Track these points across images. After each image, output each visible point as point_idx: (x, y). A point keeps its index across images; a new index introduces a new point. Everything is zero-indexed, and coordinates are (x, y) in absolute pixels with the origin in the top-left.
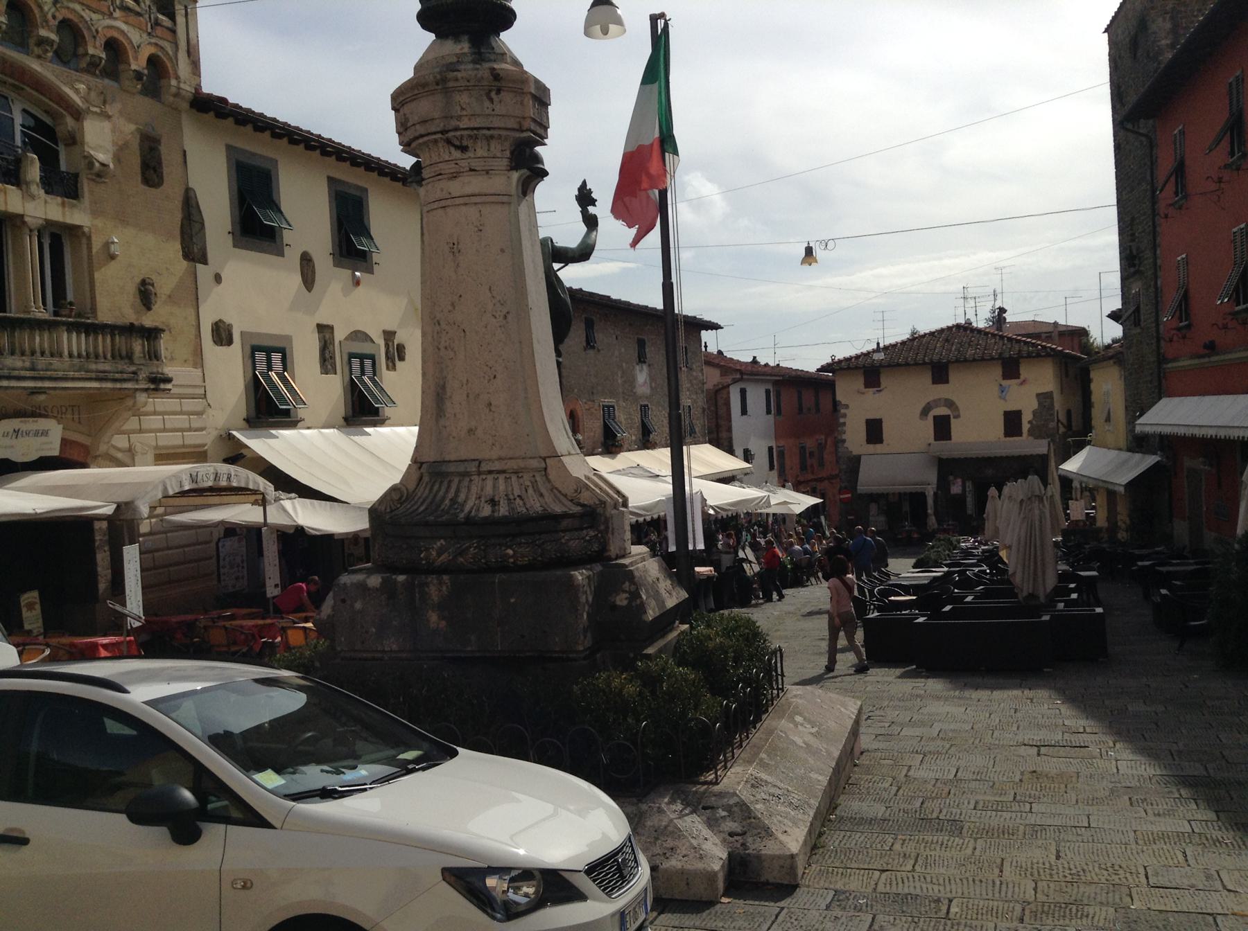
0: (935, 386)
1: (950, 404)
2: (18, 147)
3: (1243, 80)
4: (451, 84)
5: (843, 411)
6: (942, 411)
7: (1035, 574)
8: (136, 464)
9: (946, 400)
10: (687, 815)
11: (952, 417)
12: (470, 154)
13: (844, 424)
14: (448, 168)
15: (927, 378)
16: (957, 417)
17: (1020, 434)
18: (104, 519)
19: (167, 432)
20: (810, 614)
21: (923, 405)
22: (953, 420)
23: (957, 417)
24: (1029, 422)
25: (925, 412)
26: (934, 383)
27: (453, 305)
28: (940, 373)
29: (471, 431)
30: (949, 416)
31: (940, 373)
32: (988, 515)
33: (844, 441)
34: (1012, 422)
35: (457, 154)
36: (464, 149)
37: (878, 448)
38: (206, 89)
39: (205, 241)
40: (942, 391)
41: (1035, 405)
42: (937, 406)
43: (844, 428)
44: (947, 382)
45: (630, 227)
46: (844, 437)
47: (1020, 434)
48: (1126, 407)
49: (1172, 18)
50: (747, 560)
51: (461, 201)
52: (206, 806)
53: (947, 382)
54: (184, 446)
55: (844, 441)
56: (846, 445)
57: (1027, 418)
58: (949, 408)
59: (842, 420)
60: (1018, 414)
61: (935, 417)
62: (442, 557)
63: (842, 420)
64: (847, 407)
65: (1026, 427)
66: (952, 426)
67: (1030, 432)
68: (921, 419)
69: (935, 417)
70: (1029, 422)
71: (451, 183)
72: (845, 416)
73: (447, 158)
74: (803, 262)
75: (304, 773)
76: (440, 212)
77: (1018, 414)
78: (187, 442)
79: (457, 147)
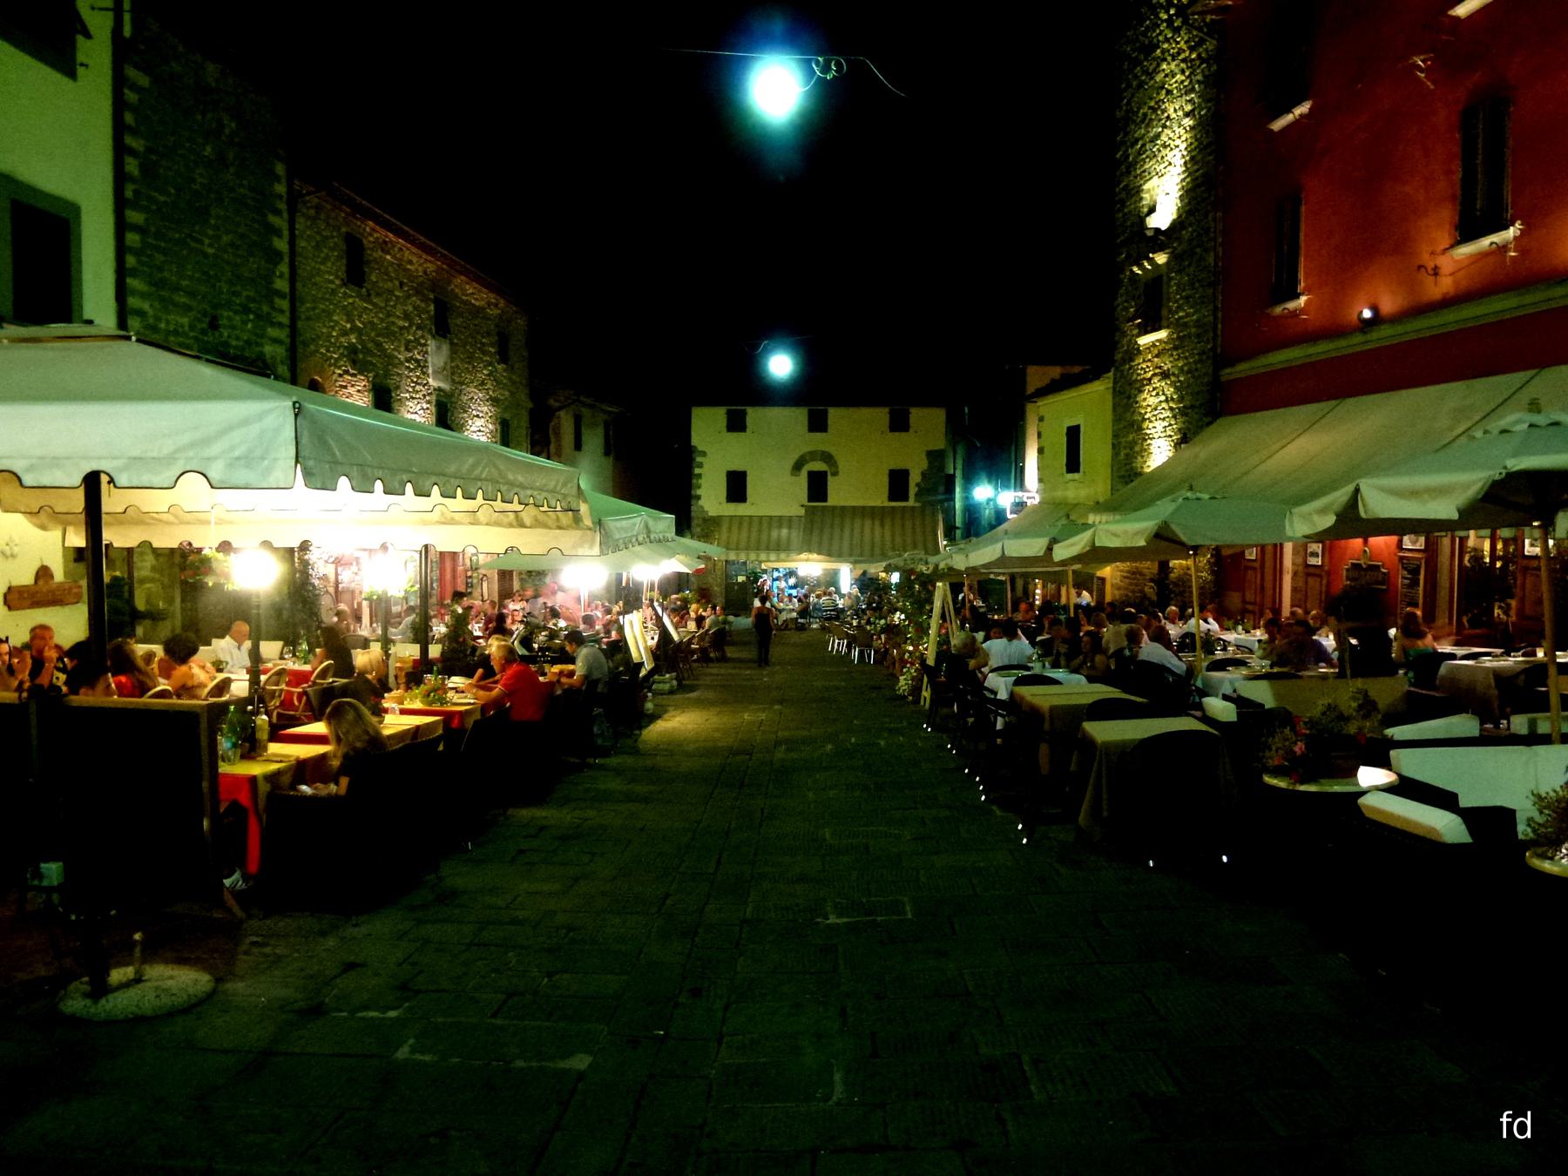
0: (729, 433)
1: (827, 458)
2: (479, 637)
5: (699, 459)
6: (818, 466)
7: (426, 558)
9: (823, 452)
10: (1020, 621)
11: (829, 474)
17: (906, 498)
18: (843, 511)
20: (406, 569)
22: (830, 478)
23: (835, 474)
25: (797, 467)
32: (1212, 539)
33: (699, 497)
39: (18, 609)
40: (818, 441)
41: (924, 464)
42: (812, 460)
43: (700, 481)
46: (699, 492)
47: (906, 498)
52: (1415, 674)
55: (699, 497)
57: (915, 478)
58: (825, 462)
59: (697, 471)
64: (704, 454)
65: (913, 490)
66: (829, 483)
68: (792, 475)
70: (917, 485)
75: (1108, 642)
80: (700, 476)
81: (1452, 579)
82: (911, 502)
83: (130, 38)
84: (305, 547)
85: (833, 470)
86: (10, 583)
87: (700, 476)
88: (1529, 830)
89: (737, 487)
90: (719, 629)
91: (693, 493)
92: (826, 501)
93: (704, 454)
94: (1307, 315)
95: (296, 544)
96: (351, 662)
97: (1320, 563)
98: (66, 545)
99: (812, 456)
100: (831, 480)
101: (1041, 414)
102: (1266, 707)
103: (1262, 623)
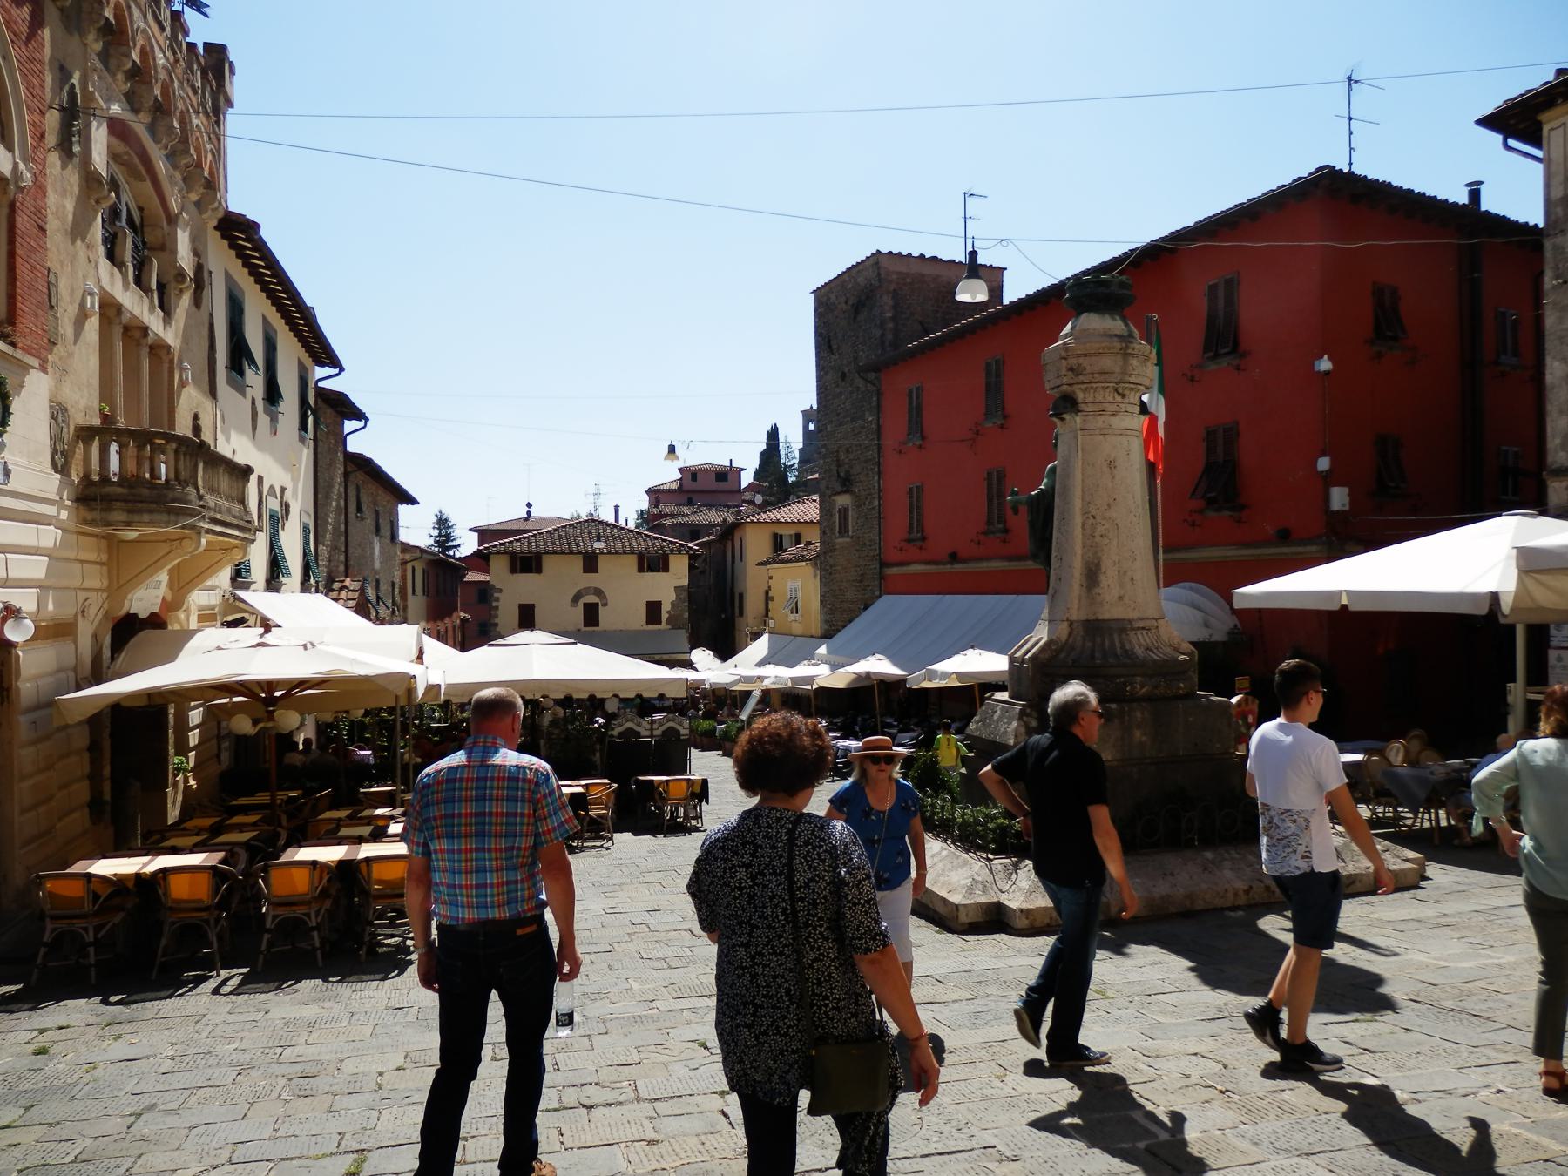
1: (599, 592)
3: (1004, 362)
4: (1130, 351)
8: (409, 621)
9: (595, 589)
12: (1126, 400)
13: (497, 608)
14: (1113, 408)
16: (605, 605)
17: (660, 623)
21: (574, 592)
23: (605, 605)
25: (576, 599)
27: (1109, 505)
29: (1121, 598)
30: (597, 604)
33: (497, 625)
34: (653, 609)
36: (1123, 396)
38: (231, 209)
40: (591, 580)
41: (673, 597)
46: (496, 621)
47: (660, 623)
49: (893, 298)
50: (815, 725)
51: (1119, 432)
55: (497, 625)
56: (498, 629)
57: (666, 608)
62: (1144, 690)
63: (494, 604)
64: (500, 591)
65: (665, 616)
67: (669, 621)
71: (1112, 418)
72: (497, 600)
73: (1111, 400)
74: (666, 458)
76: (1101, 437)
79: (1119, 394)
80: (497, 608)
82: (663, 626)
83: (1334, 365)
85: (604, 602)
86: (412, 661)
88: (1289, 833)
90: (901, 682)
92: (597, 625)
96: (1482, 616)
99: (587, 591)
100: (601, 610)
101: (548, 562)
103: (1312, 665)
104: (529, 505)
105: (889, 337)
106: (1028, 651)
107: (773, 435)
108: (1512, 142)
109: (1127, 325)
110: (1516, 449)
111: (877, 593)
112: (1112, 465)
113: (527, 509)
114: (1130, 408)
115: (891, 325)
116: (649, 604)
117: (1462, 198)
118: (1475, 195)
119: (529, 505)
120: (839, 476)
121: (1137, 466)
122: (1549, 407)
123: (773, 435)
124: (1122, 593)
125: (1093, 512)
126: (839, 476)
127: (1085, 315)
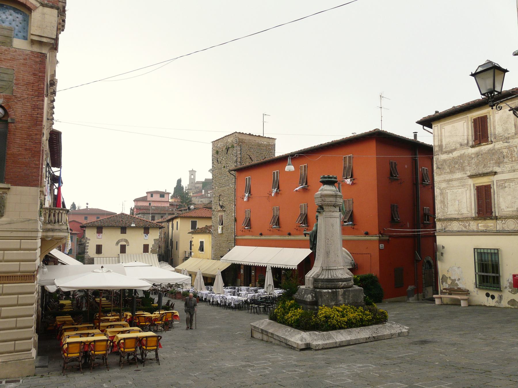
1: (126, 241)
6: (124, 243)
15: (119, 231)
19: (21, 250)
20: (143, 280)
24: (151, 248)
25: (117, 243)
26: (121, 233)
28: (123, 230)
31: (123, 230)
33: (87, 252)
35: (334, 208)
36: (335, 207)
37: (100, 255)
40: (123, 236)
41: (153, 243)
43: (88, 248)
44: (126, 233)
45: (197, 182)
46: (87, 251)
48: (212, 247)
53: (126, 233)
54: (19, 272)
55: (87, 252)
56: (88, 254)
57: (150, 247)
59: (87, 245)
60: (148, 245)
61: (121, 245)
64: (89, 240)
65: (150, 250)
67: (151, 252)
69: (121, 245)
70: (151, 248)
77: (148, 245)
78: (22, 269)
80: (88, 246)
81: (471, 202)
84: (472, 75)
87: (88, 246)
89: (99, 249)
91: (86, 251)
93: (89, 240)
94: (297, 191)
95: (473, 78)
97: (380, 245)
98: (461, 301)
102: (439, 112)
104: (87, 204)
105: (239, 160)
106: (173, 227)
107: (179, 181)
108: (425, 127)
109: (336, 188)
110: (428, 208)
111: (233, 245)
112: (333, 225)
113: (87, 205)
114: (337, 210)
115: (239, 156)
116: (144, 245)
117: (412, 137)
118: (415, 136)
119: (87, 204)
120: (220, 205)
121: (338, 226)
122: (436, 201)
123: (179, 181)
124: (335, 259)
125: (328, 238)
126: (220, 205)
127: (325, 185)
